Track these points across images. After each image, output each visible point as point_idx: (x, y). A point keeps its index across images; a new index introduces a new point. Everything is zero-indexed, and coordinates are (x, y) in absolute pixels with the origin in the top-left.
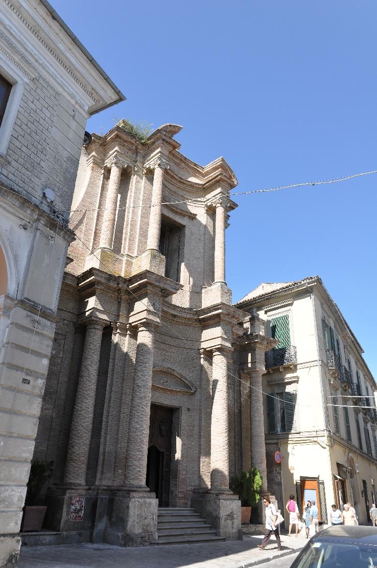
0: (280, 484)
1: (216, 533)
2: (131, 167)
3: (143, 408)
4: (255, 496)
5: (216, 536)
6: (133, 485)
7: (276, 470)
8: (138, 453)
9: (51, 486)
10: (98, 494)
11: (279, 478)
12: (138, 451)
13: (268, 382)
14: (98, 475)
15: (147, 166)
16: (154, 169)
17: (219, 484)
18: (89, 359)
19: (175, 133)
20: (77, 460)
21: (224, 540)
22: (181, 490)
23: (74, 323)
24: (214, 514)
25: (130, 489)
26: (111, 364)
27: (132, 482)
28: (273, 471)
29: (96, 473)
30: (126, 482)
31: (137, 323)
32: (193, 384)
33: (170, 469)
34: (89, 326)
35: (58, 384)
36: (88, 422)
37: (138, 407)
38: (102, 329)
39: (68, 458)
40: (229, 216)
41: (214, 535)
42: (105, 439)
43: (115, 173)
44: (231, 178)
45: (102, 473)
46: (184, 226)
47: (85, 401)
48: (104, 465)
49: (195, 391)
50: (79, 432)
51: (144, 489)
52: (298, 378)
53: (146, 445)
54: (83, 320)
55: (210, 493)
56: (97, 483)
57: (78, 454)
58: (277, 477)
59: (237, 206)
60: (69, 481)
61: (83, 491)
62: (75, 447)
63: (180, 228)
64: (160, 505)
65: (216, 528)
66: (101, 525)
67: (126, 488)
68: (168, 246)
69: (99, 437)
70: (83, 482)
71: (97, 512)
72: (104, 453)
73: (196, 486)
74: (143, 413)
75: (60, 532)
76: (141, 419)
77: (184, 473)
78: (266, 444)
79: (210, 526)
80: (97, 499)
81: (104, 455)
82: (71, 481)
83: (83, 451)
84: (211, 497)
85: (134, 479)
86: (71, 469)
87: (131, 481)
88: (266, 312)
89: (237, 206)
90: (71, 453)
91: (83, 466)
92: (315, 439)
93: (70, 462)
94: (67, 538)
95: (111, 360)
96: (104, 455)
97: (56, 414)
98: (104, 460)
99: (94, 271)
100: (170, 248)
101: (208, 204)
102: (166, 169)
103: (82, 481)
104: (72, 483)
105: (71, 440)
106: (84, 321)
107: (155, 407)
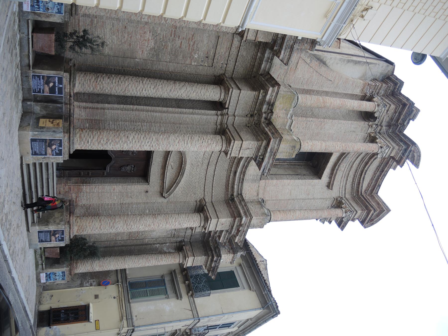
0: (81, 285)
1: (34, 222)
2: (375, 121)
3: (148, 142)
4: (52, 87)
5: (32, 223)
6: (75, 137)
7: (94, 281)
8: (105, 139)
9: (72, 62)
10: (66, 104)
11: (87, 285)
12: (107, 140)
13: (175, 271)
14: (84, 104)
15: (377, 137)
16: (377, 143)
17: (78, 224)
18: (192, 90)
19: (412, 162)
20: (97, 82)
21: (28, 230)
22: (72, 187)
23: (224, 74)
24: (51, 220)
25: (72, 133)
26: (188, 110)
27: (78, 135)
28: (93, 279)
29: (86, 102)
30: (78, 130)
31: (229, 133)
32: (169, 195)
33: (91, 177)
34: (222, 88)
35: (166, 62)
36: (133, 91)
37: (148, 137)
38: (220, 100)
39: (98, 74)
40: (330, 222)
41: (33, 222)
42: (117, 109)
43: (367, 106)
44: (371, 221)
45: (85, 108)
46: (320, 178)
47: (152, 87)
48: (93, 108)
49: (164, 197)
50: (123, 83)
51: (71, 147)
52: (181, 297)
53: (112, 148)
54: (228, 81)
55: (70, 216)
56: (76, 103)
57: (102, 83)
58: (88, 282)
59: (342, 229)
60: (78, 76)
61: (69, 90)
62: (108, 80)
63: (318, 174)
64: (58, 164)
65: (39, 222)
66: (37, 108)
67: (72, 130)
68: (299, 165)
69: (119, 103)
70: (76, 90)
71: (49, 104)
72: (104, 109)
73: (76, 202)
74: (143, 143)
75: (31, 69)
76: (137, 141)
77: (88, 190)
78: (117, 270)
79: (41, 217)
80: (62, 103)
81: (102, 109)
82: (77, 78)
83: (105, 88)
84: (67, 216)
85: (80, 137)
86: (88, 77)
87: (79, 134)
88: (240, 265)
89: (342, 229)
90: (103, 76)
91: (92, 89)
92: (125, 318)
93: (94, 76)
94: (26, 77)
95: (191, 110)
96: (102, 109)
97: (138, 62)
98: (97, 108)
99: (276, 88)
100: (297, 166)
101: (343, 201)
102: (378, 154)
103: (78, 88)
104: (75, 78)
105: (115, 76)
106: (227, 83)
107: (148, 155)
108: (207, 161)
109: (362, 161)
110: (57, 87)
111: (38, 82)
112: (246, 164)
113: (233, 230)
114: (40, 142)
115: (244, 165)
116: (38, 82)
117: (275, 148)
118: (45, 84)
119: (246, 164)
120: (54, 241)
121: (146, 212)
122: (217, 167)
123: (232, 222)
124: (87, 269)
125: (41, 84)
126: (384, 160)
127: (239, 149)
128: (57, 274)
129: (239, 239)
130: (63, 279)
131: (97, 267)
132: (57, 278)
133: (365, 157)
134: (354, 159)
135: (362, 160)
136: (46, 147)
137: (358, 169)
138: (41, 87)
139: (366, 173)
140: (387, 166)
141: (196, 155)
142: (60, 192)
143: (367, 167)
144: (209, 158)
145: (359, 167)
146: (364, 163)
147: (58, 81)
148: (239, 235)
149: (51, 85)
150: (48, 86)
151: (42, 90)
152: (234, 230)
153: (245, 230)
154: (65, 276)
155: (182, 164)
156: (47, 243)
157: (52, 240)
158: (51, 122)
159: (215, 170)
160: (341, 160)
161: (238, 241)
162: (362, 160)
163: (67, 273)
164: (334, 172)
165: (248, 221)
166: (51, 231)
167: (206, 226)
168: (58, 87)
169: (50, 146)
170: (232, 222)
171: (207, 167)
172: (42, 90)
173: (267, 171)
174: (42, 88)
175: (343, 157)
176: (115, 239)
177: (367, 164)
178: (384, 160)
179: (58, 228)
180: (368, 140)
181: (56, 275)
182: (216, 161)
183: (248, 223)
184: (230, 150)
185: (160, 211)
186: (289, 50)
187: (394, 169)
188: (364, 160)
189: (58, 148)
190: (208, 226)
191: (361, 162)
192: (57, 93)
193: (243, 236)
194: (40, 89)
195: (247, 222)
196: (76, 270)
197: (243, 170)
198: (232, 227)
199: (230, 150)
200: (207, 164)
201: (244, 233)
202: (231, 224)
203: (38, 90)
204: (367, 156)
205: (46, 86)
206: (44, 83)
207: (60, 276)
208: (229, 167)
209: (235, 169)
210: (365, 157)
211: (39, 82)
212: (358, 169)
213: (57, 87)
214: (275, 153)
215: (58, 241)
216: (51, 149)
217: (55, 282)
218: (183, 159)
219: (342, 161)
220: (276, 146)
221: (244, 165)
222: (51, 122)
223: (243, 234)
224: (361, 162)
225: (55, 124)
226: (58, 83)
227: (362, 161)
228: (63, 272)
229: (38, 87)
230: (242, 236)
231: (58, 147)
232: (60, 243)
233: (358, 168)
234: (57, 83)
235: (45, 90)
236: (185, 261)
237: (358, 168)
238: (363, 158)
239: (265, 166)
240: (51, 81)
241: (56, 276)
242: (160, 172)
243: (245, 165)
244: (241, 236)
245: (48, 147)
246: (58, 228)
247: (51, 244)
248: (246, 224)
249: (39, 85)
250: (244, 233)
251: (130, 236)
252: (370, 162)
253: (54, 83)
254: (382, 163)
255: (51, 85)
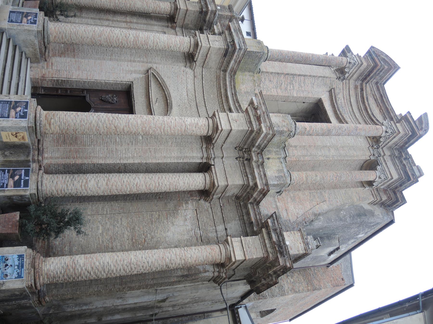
4: (17, 180)
108: (195, 103)
109: (361, 111)
110: (22, 179)
111: (3, 176)
112: (233, 91)
113: (253, 123)
114: (4, 103)
115: (233, 94)
116: (3, 176)
117: (236, 26)
118: (10, 178)
119: (233, 91)
120: (13, 118)
121: (138, 139)
122: (207, 108)
123: (246, 117)
124: (63, 262)
125: (6, 178)
126: (382, 110)
127: (207, 40)
128: (9, 262)
129: (266, 127)
130: (19, 276)
131: (81, 259)
132: (9, 271)
133: (358, 106)
134: (350, 108)
135: (360, 110)
136: (10, 109)
137: (365, 119)
138: (5, 182)
139: (374, 116)
140: (391, 112)
141: (179, 95)
142: (26, 60)
143: (369, 110)
144: (194, 100)
145: (364, 117)
146: (363, 111)
147: (25, 173)
148: (262, 122)
149: (17, 178)
150: (13, 179)
151: (5, 184)
152: (254, 123)
153: (264, 110)
154: (22, 266)
155: (167, 100)
156: (3, 120)
157: (10, 115)
158: (15, 136)
159: (207, 111)
160: (335, 104)
161: (266, 130)
162: (360, 110)
163: (27, 261)
164: (341, 117)
165: (260, 98)
166: (11, 102)
167: (215, 120)
168: (24, 180)
169: (15, 108)
170: (246, 117)
171: (197, 110)
172: (5, 184)
173: (243, 44)
174: (6, 182)
175: (334, 99)
176: (110, 246)
177: (366, 109)
178: (382, 110)
179: (21, 98)
180: (338, 74)
181: (8, 262)
182: (203, 102)
183: (261, 100)
184: (198, 38)
185: (156, 137)
186: (212, 3)
187: (401, 114)
188: (361, 108)
189: (23, 111)
190: (218, 120)
191: (360, 112)
192: (22, 186)
193: (266, 118)
194: (3, 184)
195: (259, 100)
196: (43, 264)
197: (235, 98)
198: (250, 122)
199: (198, 38)
200: (196, 107)
201: (265, 114)
202: (247, 120)
203: (2, 185)
204: (359, 103)
205: (11, 179)
206: (9, 177)
207: (15, 266)
208: (221, 110)
209: (228, 107)
210: (358, 106)
211: (3, 176)
212: (365, 119)
213: (22, 179)
214: (239, 29)
215: (18, 117)
216: (16, 111)
217: (4, 283)
218: (166, 93)
219: (337, 104)
220: (236, 25)
221: (233, 94)
222: (15, 136)
223: (266, 116)
224: (360, 112)
225: (20, 137)
226: (24, 175)
227: (361, 111)
228: (21, 257)
229: (2, 182)
230: (265, 119)
231: (23, 109)
232: (20, 120)
233: (363, 118)
234: (23, 176)
235: (9, 184)
236: (228, 246)
237: (363, 118)
238: (359, 108)
239: (238, 43)
240: (17, 174)
241: (7, 265)
242: (146, 112)
243: (234, 93)
244: (265, 122)
245: (12, 109)
246: (21, 98)
247: (8, 121)
248: (260, 104)
249: (3, 180)
250: (265, 114)
251: (134, 241)
252: (367, 105)
253: (20, 176)
254: (384, 114)
255: (17, 178)
